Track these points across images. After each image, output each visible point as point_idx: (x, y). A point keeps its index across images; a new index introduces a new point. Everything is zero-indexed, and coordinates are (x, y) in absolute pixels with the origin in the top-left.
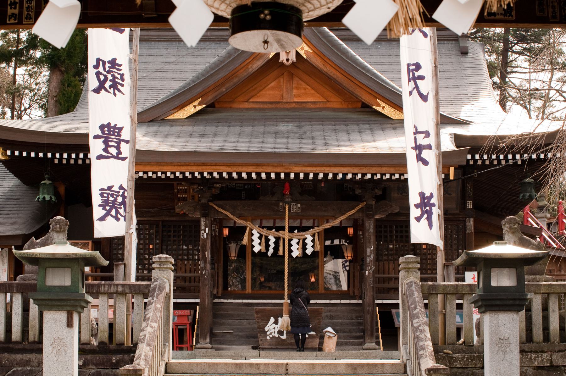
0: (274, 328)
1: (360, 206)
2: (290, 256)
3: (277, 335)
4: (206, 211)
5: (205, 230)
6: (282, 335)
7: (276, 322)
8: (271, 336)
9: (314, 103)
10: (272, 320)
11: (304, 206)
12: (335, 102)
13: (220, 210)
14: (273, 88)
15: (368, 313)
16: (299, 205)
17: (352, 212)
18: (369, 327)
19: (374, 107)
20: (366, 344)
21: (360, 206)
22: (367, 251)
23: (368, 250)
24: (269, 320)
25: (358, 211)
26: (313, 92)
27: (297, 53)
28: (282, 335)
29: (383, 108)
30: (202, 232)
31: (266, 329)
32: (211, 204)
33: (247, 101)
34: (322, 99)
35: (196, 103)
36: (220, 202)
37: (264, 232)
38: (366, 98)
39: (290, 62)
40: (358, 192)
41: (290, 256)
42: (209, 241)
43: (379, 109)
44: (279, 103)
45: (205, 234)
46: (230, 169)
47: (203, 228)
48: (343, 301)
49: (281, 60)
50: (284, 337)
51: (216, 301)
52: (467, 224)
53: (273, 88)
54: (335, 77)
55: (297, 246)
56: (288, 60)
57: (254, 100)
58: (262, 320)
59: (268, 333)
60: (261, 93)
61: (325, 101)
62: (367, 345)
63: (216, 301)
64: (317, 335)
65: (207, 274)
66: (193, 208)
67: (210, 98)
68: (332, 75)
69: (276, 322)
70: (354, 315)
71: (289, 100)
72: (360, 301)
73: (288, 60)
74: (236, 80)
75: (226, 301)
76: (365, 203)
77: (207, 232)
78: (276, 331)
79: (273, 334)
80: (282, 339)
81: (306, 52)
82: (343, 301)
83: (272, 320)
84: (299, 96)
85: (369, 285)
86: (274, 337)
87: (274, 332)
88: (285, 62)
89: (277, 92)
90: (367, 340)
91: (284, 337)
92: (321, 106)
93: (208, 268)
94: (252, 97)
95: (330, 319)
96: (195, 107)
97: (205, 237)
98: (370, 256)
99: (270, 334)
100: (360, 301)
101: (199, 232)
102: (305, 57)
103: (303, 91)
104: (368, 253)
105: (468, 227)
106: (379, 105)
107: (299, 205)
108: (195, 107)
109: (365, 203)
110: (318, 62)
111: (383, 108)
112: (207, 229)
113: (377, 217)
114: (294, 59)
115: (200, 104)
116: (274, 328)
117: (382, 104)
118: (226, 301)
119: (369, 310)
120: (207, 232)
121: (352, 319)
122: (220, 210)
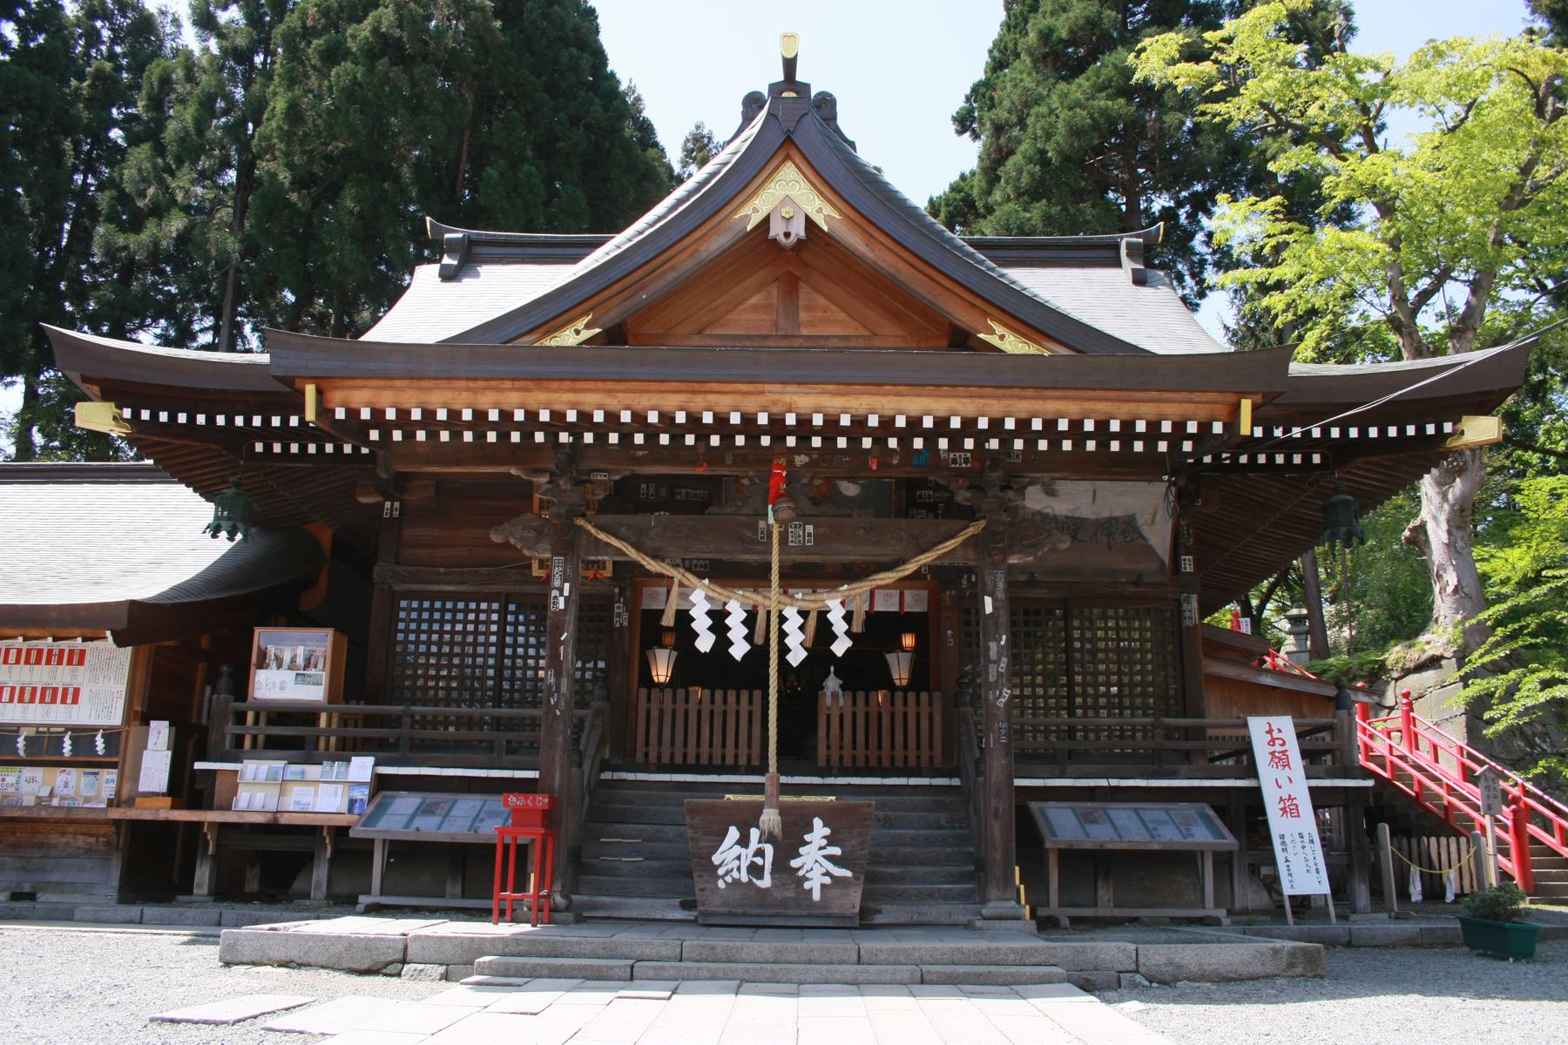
0: (739, 858)
1: (971, 531)
2: (783, 663)
3: (744, 878)
4: (568, 542)
5: (561, 590)
6: (761, 877)
7: (744, 841)
8: (728, 879)
9: (846, 338)
10: (733, 833)
11: (821, 530)
12: (890, 334)
13: (602, 536)
14: (755, 308)
15: (996, 817)
16: (810, 528)
17: (950, 544)
18: (998, 856)
19: (981, 336)
20: (991, 904)
21: (971, 531)
22: (988, 649)
23: (993, 646)
24: (723, 834)
25: (964, 544)
26: (842, 316)
27: (808, 220)
28: (761, 877)
29: (1002, 337)
30: (555, 593)
31: (716, 859)
32: (580, 522)
33: (700, 332)
34: (862, 331)
35: (580, 324)
36: (604, 519)
37: (719, 593)
38: (962, 315)
39: (793, 239)
40: (963, 496)
41: (783, 663)
42: (571, 619)
43: (993, 340)
44: (767, 337)
45: (561, 600)
46: (614, 402)
47: (557, 583)
48: (913, 781)
49: (772, 234)
50: (766, 882)
51: (606, 776)
52: (1185, 606)
53: (756, 308)
54: (892, 271)
55: (801, 637)
56: (787, 235)
57: (719, 331)
58: (705, 834)
59: (721, 871)
60: (730, 316)
61: (867, 333)
62: (992, 908)
63: (606, 776)
64: (856, 878)
65: (562, 703)
66: (533, 534)
67: (613, 316)
68: (884, 265)
69: (744, 841)
70: (943, 817)
71: (789, 332)
72: (956, 782)
73: (787, 235)
74: (671, 276)
75: (631, 776)
76: (982, 523)
77: (566, 593)
78: (744, 865)
79: (735, 874)
80: (759, 890)
81: (828, 218)
82: (913, 781)
83: (733, 833)
84: (812, 324)
85: (997, 741)
86: (737, 882)
87: (739, 869)
88: (781, 238)
89: (764, 317)
90: (993, 892)
91: (766, 882)
92: (861, 343)
93: (564, 689)
94: (709, 325)
95: (884, 826)
96: (578, 332)
97: (562, 605)
98: (997, 662)
99: (727, 873)
100: (956, 782)
101: (547, 596)
102: (825, 228)
103: (820, 314)
104: (993, 654)
105: (1187, 614)
106: (992, 332)
107: (810, 528)
108: (578, 332)
109: (982, 523)
110: (854, 240)
111: (1002, 337)
112: (567, 586)
113: (1013, 560)
114: (802, 234)
115: (588, 326)
116: (739, 858)
117: (999, 330)
118: (631, 776)
119: (997, 809)
120: (566, 593)
121: (941, 827)
122: (602, 536)
